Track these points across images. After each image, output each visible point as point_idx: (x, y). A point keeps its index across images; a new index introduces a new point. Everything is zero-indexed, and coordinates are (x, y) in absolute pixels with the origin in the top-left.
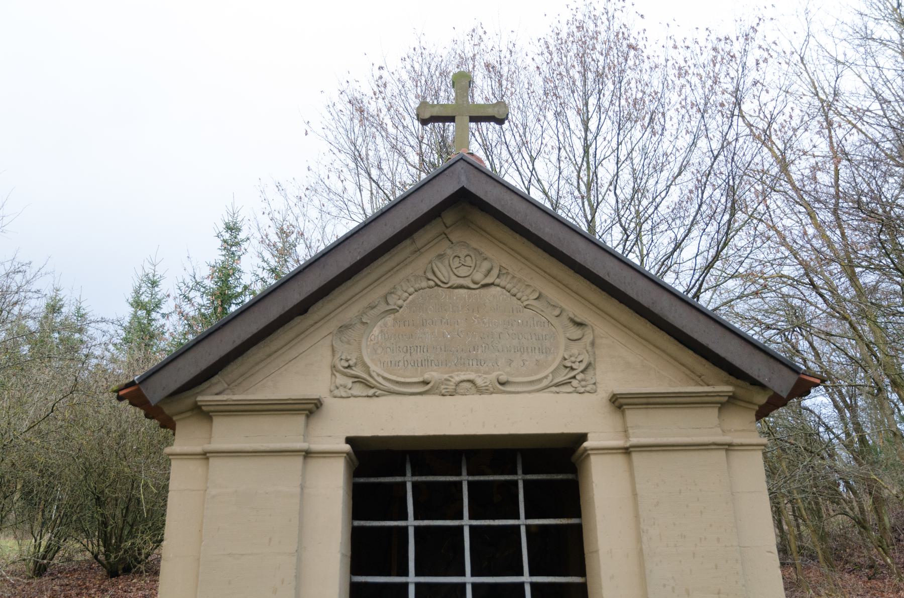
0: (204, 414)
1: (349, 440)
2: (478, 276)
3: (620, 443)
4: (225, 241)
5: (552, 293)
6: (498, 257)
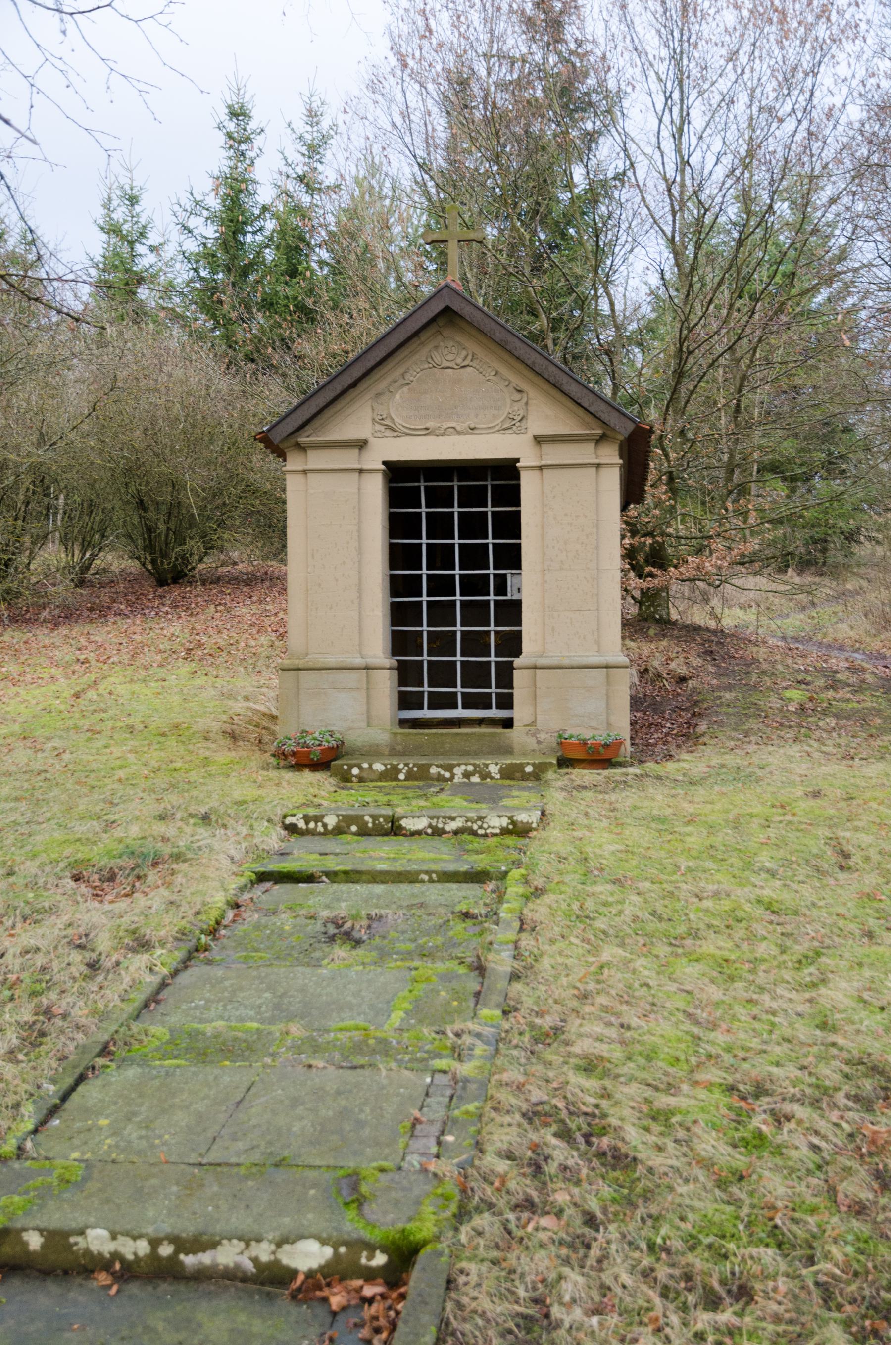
0: (302, 448)
1: (384, 463)
2: (459, 361)
3: (537, 464)
4: (229, 136)
5: (504, 371)
6: (472, 346)
